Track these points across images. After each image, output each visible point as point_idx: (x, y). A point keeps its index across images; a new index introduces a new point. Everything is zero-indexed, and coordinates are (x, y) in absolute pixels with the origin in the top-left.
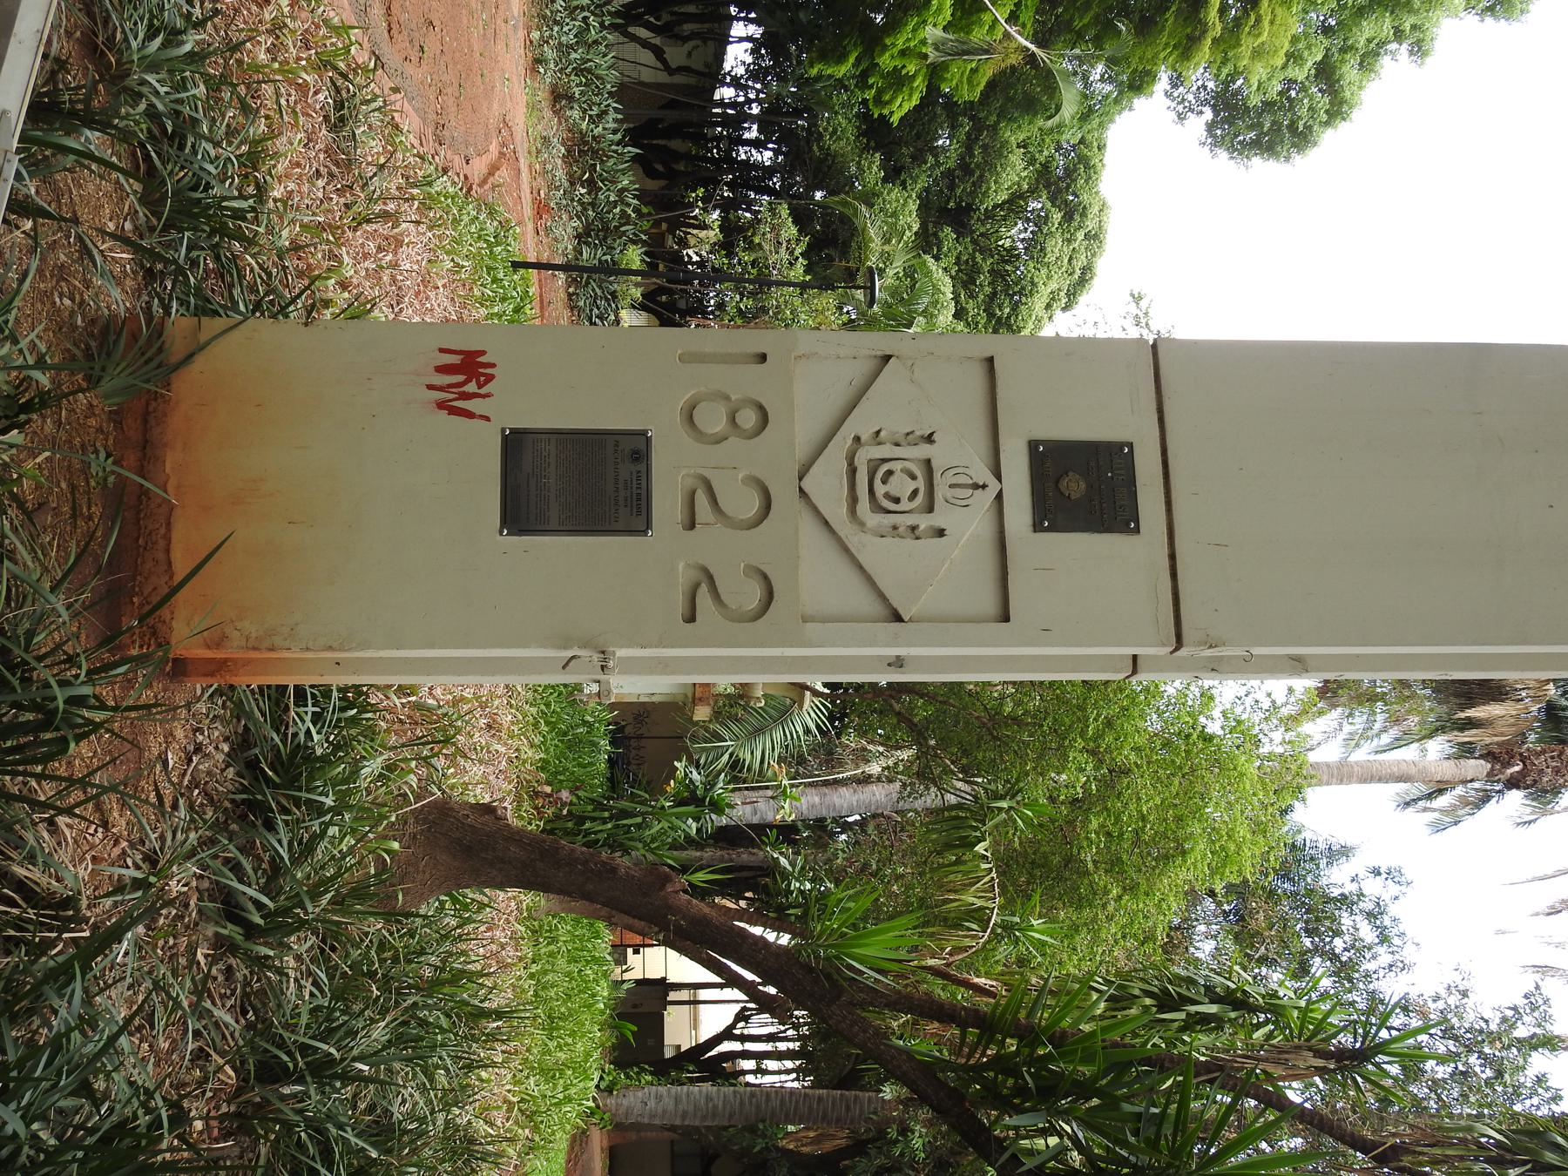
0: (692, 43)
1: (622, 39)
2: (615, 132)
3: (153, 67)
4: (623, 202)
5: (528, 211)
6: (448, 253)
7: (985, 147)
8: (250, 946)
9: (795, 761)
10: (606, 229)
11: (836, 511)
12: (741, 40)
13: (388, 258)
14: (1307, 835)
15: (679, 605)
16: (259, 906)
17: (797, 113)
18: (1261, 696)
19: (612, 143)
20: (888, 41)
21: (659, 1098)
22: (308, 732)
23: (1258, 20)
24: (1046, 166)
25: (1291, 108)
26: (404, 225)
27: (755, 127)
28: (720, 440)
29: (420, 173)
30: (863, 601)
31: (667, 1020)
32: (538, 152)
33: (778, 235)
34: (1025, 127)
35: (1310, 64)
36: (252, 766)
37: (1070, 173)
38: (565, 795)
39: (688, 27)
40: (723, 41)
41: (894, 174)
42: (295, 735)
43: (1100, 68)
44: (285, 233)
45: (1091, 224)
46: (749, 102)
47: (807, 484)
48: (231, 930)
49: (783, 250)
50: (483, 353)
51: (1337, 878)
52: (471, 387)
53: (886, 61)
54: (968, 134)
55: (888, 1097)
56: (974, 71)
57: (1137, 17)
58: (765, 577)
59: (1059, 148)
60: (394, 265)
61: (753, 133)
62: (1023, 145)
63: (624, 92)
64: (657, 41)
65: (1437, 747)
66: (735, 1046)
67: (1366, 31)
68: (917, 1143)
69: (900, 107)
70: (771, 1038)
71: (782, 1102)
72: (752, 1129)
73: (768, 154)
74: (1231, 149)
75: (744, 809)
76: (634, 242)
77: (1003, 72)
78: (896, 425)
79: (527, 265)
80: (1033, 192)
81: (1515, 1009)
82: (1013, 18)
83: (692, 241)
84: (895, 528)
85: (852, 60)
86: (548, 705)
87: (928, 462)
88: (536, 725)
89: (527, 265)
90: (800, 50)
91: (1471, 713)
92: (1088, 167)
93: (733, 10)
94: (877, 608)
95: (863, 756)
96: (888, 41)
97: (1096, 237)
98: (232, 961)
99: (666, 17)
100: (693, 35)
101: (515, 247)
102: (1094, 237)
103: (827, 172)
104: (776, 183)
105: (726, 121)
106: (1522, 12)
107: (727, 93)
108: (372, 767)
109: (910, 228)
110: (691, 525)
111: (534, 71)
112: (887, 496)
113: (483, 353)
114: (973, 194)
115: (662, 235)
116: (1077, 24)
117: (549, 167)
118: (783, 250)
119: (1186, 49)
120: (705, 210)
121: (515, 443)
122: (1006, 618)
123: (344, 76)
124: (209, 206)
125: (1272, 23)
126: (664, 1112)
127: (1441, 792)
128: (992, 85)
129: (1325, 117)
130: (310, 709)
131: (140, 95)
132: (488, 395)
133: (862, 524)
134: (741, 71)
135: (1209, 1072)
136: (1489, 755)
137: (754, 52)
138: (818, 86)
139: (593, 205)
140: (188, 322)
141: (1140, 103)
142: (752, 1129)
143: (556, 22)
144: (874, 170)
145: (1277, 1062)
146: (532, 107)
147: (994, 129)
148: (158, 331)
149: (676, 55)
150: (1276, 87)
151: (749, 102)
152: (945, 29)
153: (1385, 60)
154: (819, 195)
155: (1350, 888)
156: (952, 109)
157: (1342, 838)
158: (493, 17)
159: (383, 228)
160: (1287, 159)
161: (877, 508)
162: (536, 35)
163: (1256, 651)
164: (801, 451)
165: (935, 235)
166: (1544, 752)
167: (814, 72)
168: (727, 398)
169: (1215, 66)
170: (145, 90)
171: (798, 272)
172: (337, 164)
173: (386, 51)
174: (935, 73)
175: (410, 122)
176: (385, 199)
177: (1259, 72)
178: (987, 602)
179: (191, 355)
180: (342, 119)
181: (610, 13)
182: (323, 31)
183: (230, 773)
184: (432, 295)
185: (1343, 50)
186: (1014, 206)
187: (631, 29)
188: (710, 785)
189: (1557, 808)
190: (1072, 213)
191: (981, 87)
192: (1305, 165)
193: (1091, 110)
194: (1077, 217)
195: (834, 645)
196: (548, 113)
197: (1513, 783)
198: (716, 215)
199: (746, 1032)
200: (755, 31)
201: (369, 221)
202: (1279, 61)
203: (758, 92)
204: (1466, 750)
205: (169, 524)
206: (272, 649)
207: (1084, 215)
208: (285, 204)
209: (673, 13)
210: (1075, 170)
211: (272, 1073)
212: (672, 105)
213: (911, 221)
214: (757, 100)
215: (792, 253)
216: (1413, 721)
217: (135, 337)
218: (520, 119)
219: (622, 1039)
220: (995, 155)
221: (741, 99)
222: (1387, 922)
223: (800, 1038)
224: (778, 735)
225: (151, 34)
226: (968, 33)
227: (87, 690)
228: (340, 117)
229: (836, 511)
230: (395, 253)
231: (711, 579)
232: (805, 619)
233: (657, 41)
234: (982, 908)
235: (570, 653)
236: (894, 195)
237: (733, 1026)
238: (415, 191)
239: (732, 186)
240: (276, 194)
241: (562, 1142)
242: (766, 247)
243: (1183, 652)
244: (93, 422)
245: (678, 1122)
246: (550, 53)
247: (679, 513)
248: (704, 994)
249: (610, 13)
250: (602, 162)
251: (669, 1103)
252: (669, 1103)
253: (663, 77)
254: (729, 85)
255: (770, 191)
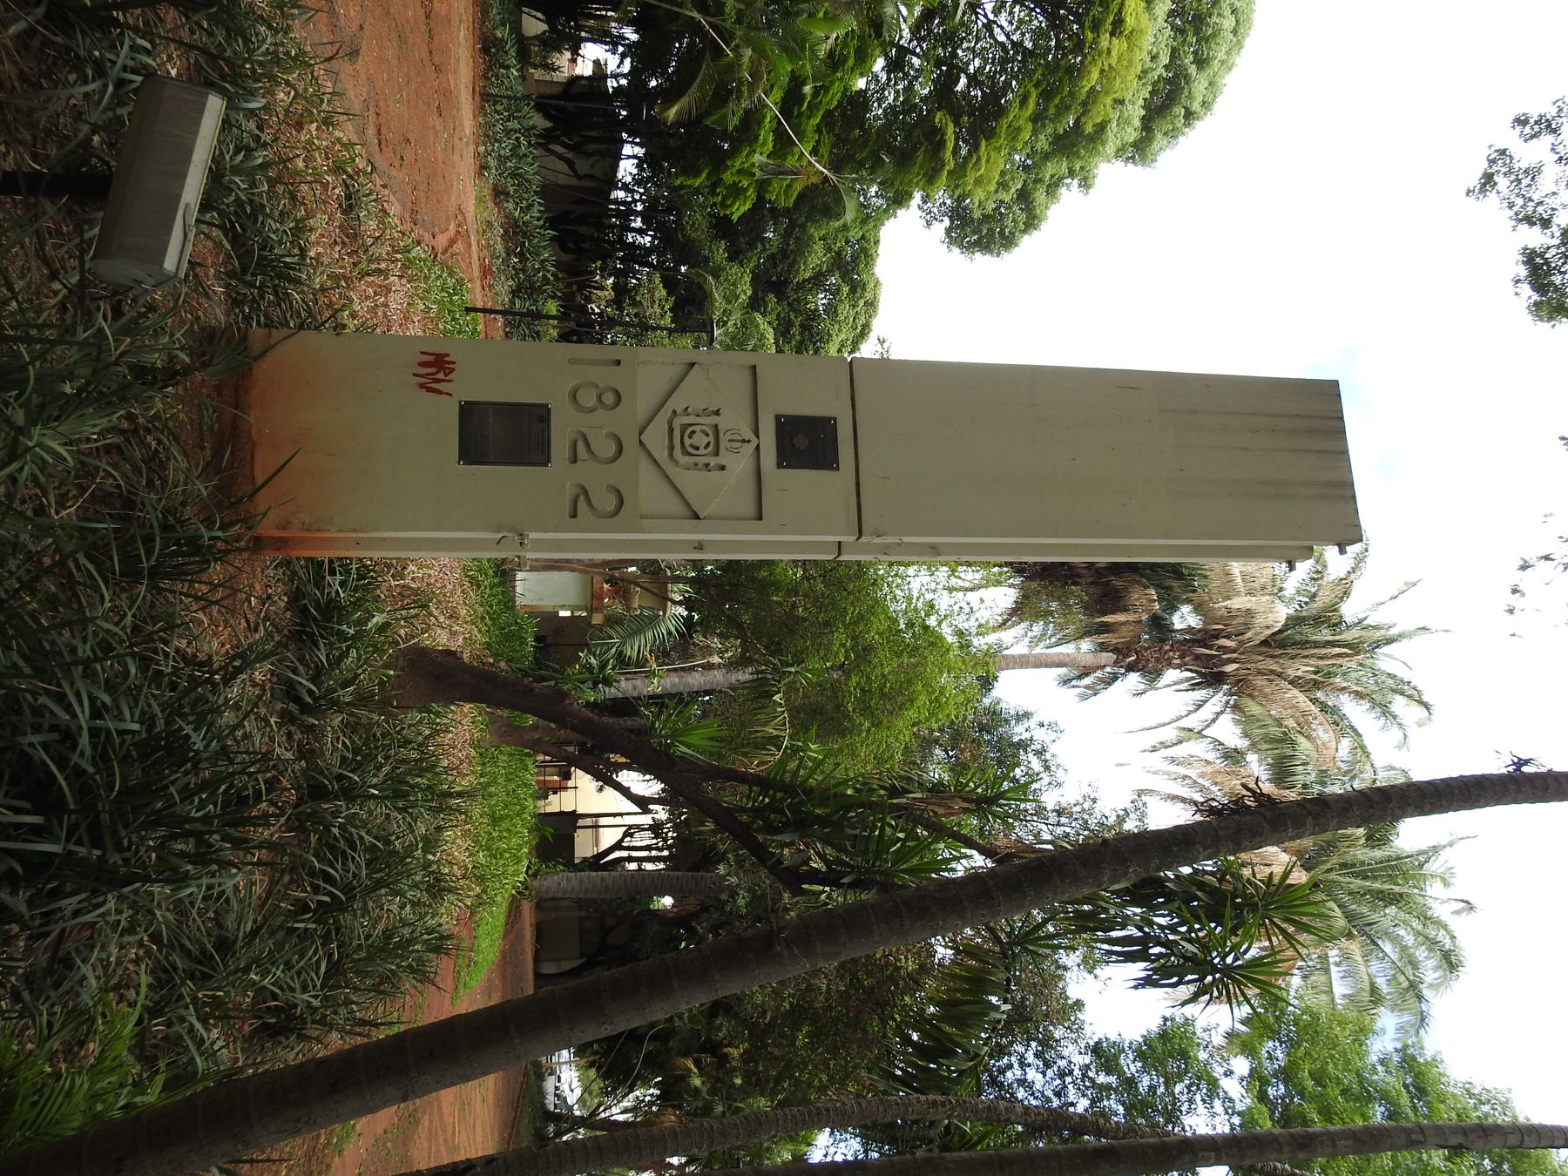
0: (595, 158)
1: (544, 153)
2: (539, 219)
3: (236, 170)
4: (544, 269)
5: (476, 273)
6: (421, 299)
7: (797, 239)
8: (305, 717)
9: (663, 655)
10: (532, 287)
11: (661, 454)
12: (629, 157)
13: (382, 299)
14: (1003, 705)
15: (567, 510)
16: (310, 692)
17: (668, 211)
18: (963, 604)
19: (537, 227)
20: (729, 163)
21: (569, 880)
22: (337, 591)
23: (979, 159)
24: (839, 254)
25: (1001, 220)
26: (392, 278)
27: (639, 219)
28: (592, 410)
29: (402, 244)
30: (677, 507)
31: (576, 840)
32: (484, 231)
33: (653, 295)
34: (824, 226)
35: (1013, 190)
36: (304, 611)
37: (855, 259)
38: (502, 664)
39: (592, 147)
40: (617, 157)
41: (735, 255)
42: (329, 594)
43: (874, 189)
44: (317, 280)
45: (868, 295)
46: (635, 201)
47: (644, 438)
48: (293, 707)
49: (656, 306)
50: (448, 355)
51: (1019, 732)
52: (441, 376)
53: (728, 177)
54: (786, 230)
55: (722, 872)
56: (789, 186)
57: (898, 154)
58: (619, 492)
59: (847, 242)
60: (386, 305)
61: (638, 223)
62: (823, 239)
63: (546, 191)
64: (570, 155)
65: (1086, 645)
66: (625, 854)
67: (1050, 169)
68: (741, 902)
69: (739, 209)
70: (648, 848)
71: (653, 881)
72: (632, 900)
73: (648, 239)
74: (961, 246)
75: (626, 687)
76: (552, 298)
77: (807, 187)
78: (697, 404)
79: (476, 310)
80: (830, 272)
81: (1125, 810)
82: (814, 152)
83: (594, 297)
84: (696, 465)
85: (704, 175)
86: (491, 606)
87: (716, 426)
88: (483, 618)
89: (476, 310)
90: (671, 166)
91: (1109, 619)
92: (867, 256)
93: (625, 136)
94: (684, 511)
95: (708, 651)
96: (729, 163)
97: (872, 304)
98: (292, 728)
99: (576, 139)
100: (596, 153)
101: (467, 297)
102: (871, 305)
103: (687, 251)
104: (654, 259)
105: (618, 214)
106: (1152, 161)
107: (621, 194)
108: (378, 619)
109: (745, 293)
110: (574, 461)
111: (481, 174)
112: (691, 446)
113: (448, 355)
114: (789, 271)
115: (573, 294)
116: (858, 157)
117: (491, 243)
118: (656, 306)
119: (930, 178)
120: (602, 277)
121: (468, 411)
122: (760, 518)
123: (351, 177)
124: (273, 260)
125: (987, 161)
126: (573, 889)
127: (1087, 675)
128: (802, 196)
129: (1023, 227)
130: (338, 577)
131: (232, 190)
132: (451, 381)
133: (676, 462)
134: (629, 179)
135: (899, 810)
136: (1116, 650)
137: (639, 166)
138: (683, 192)
139: (523, 270)
140: (263, 331)
141: (901, 213)
142: (632, 900)
143: (496, 140)
144: (720, 252)
145: (940, 805)
146: (480, 200)
147: (803, 227)
148: (244, 338)
149: (583, 166)
150: (991, 206)
151: (635, 201)
152: (768, 157)
153: (1063, 190)
154: (683, 269)
155: (1026, 735)
156: (775, 213)
157: (1026, 706)
158: (451, 136)
159: (378, 280)
160: (998, 254)
161: (685, 452)
162: (481, 149)
163: (906, 539)
164: (641, 418)
165: (763, 299)
166: (1149, 648)
167: (678, 182)
168: (597, 386)
169: (952, 188)
170: (234, 186)
171: (667, 320)
172: (348, 237)
173: (378, 160)
174: (762, 186)
175: (394, 209)
176: (378, 260)
177: (979, 195)
178: (749, 508)
179: (265, 352)
180: (350, 206)
181: (535, 135)
182: (338, 147)
183: (288, 614)
184: (411, 327)
185: (1036, 181)
186: (818, 280)
187: (551, 147)
188: (603, 666)
189: (1159, 685)
190: (857, 288)
191: (794, 197)
192: (1010, 258)
193: (868, 217)
194: (859, 290)
195: (659, 532)
196: (491, 205)
197: (1131, 668)
198: (611, 281)
199: (632, 844)
200: (639, 151)
201: (369, 275)
202: (992, 188)
203: (641, 194)
204: (1103, 647)
205: (253, 455)
206: (319, 531)
207: (864, 289)
208: (317, 260)
209: (581, 136)
210: (858, 258)
211: (317, 792)
212: (580, 201)
213: (745, 290)
214: (640, 200)
215: (663, 308)
216: (1071, 629)
217: (229, 341)
218: (470, 207)
219: (544, 838)
220: (804, 245)
221: (629, 199)
222: (1048, 756)
223: (669, 848)
224: (649, 635)
225: (237, 151)
226: (785, 160)
227: (219, 534)
228: (350, 204)
229: (661, 454)
230: (386, 297)
231: (586, 492)
232: (642, 517)
233: (570, 155)
234: (778, 736)
235: (500, 536)
236: (734, 270)
237: (622, 840)
238: (399, 256)
239: (622, 260)
240: (312, 254)
241: (503, 900)
242: (645, 304)
243: (863, 539)
244: (204, 390)
245: (582, 896)
246: (492, 162)
247: (567, 454)
248: (603, 821)
249: (535, 135)
250: (530, 240)
251: (575, 883)
252: (575, 883)
253: (574, 182)
254: (620, 189)
255: (650, 265)
